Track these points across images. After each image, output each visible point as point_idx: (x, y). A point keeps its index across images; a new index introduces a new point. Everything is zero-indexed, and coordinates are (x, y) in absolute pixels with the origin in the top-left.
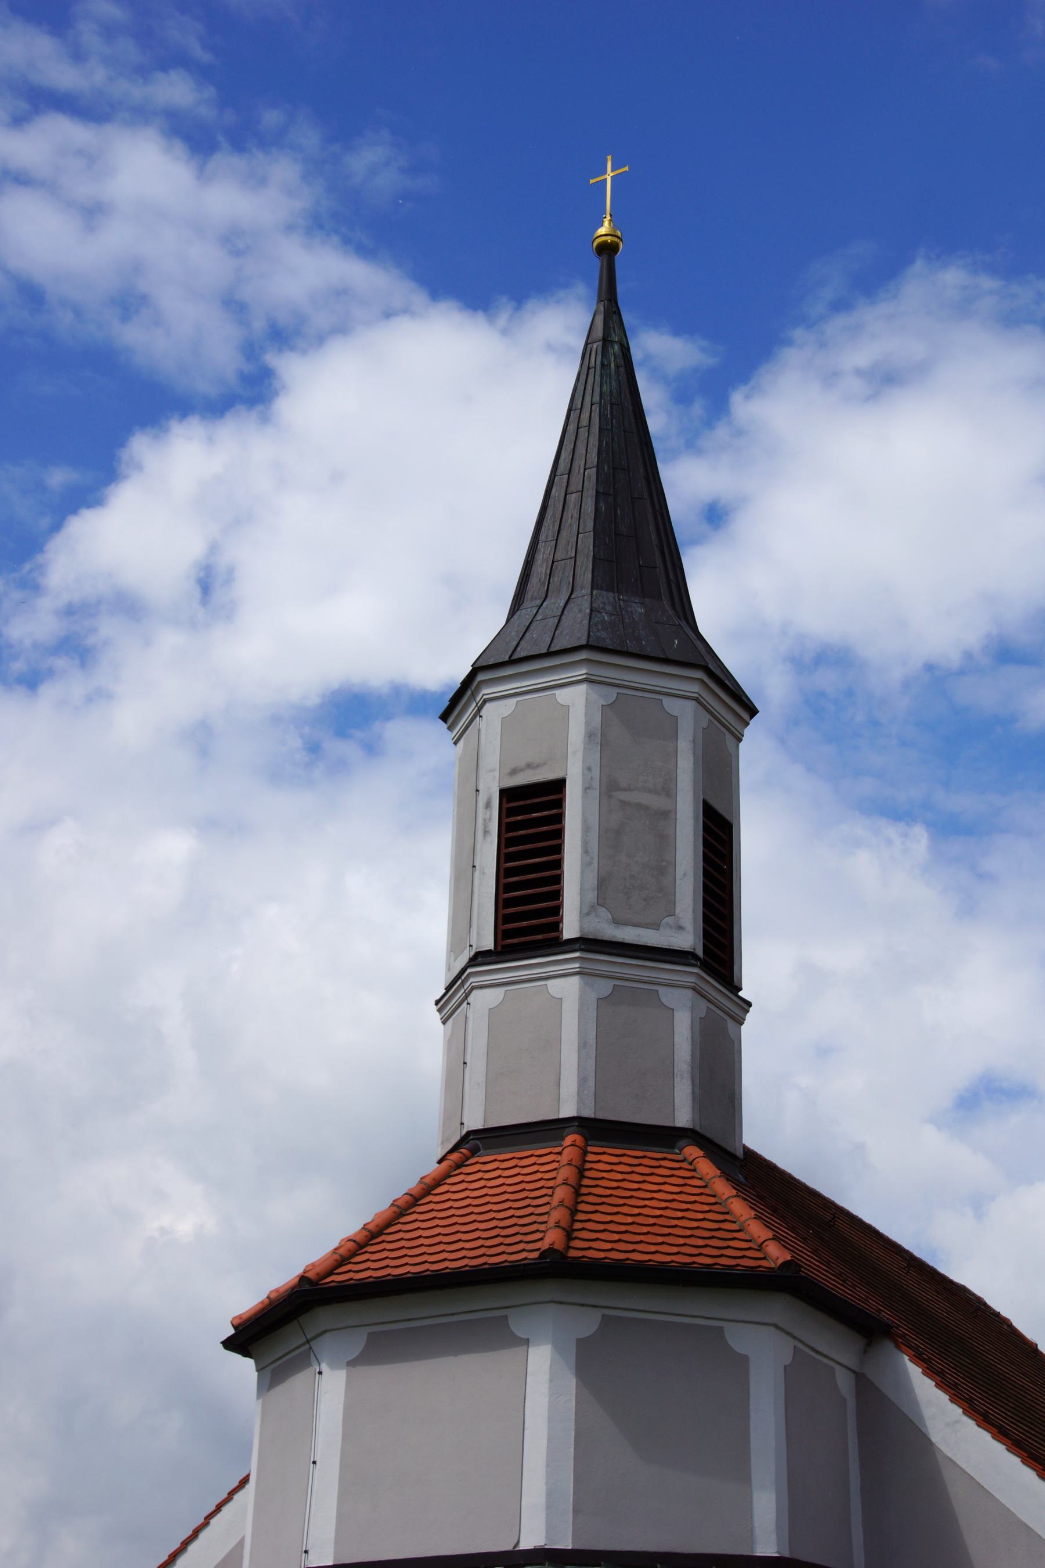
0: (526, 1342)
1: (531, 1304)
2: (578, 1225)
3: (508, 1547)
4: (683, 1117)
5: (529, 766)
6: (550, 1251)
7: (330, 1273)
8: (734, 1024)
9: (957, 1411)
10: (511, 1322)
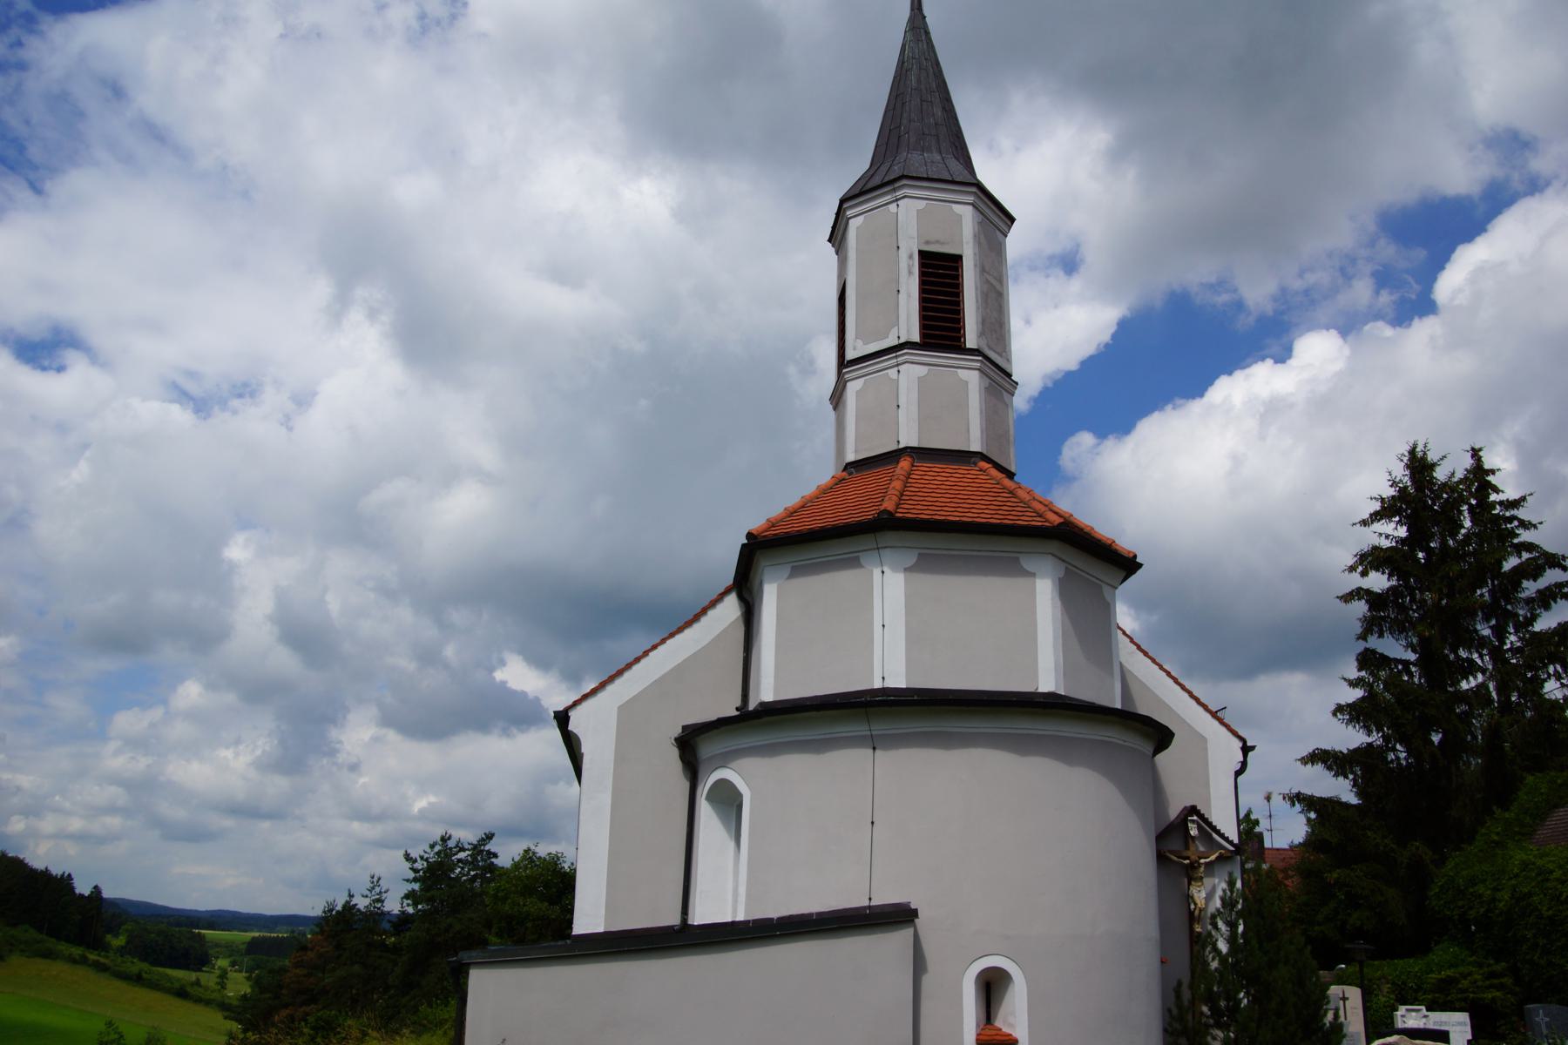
0: (1033, 575)
1: (865, 550)
2: (902, 502)
3: (1033, 690)
4: (975, 446)
5: (937, 242)
6: (885, 511)
7: (763, 532)
8: (1009, 395)
9: (686, 657)
10: (862, 561)
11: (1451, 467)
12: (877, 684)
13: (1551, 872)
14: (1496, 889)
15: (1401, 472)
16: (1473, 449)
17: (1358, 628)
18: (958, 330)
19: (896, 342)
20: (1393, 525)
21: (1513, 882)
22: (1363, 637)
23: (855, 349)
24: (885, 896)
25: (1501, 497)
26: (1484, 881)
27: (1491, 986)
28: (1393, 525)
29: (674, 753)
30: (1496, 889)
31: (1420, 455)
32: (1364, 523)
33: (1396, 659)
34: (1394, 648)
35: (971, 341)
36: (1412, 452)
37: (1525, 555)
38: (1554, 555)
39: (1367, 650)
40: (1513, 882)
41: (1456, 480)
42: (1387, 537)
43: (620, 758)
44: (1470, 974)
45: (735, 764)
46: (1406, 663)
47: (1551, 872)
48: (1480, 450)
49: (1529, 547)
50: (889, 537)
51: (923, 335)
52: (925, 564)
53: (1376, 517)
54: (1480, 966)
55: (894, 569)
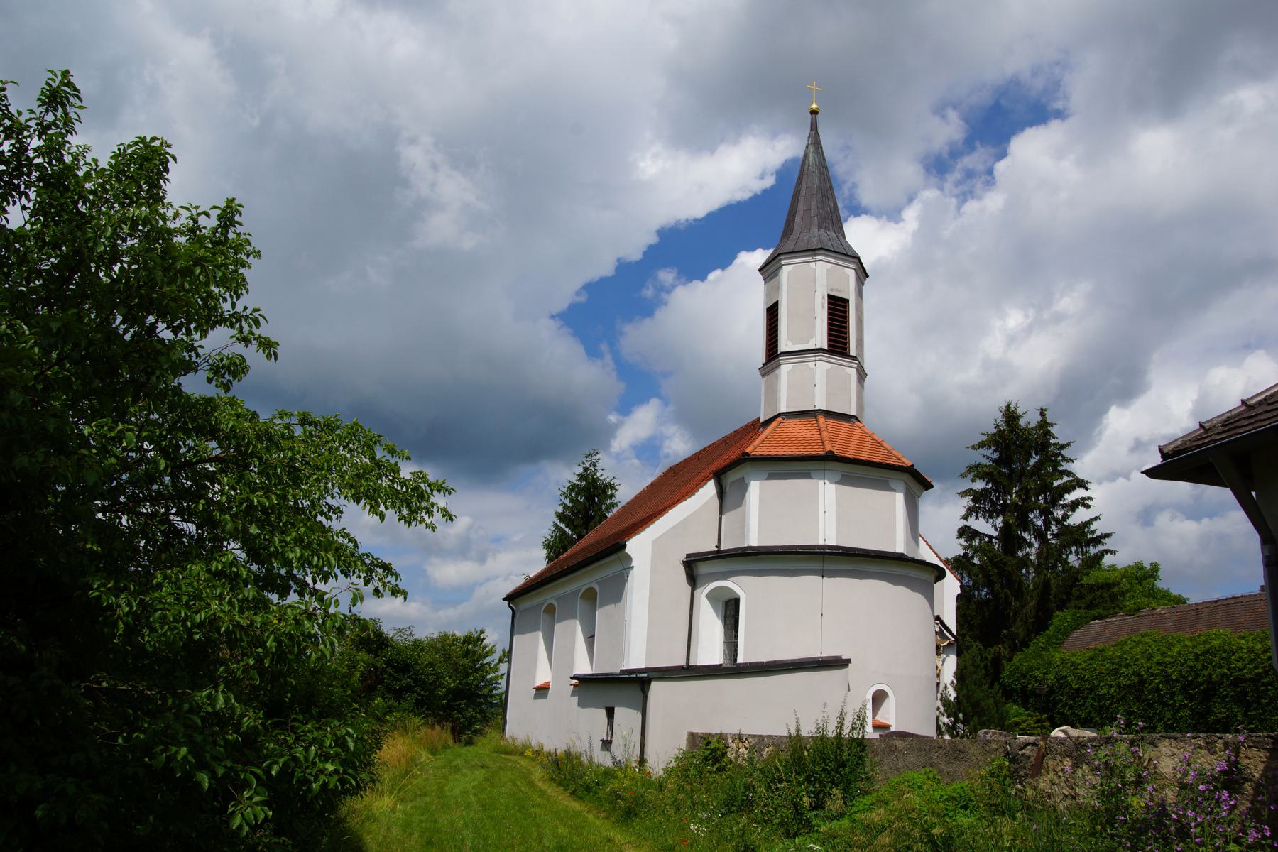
5: (837, 290)
11: (1030, 419)
12: (821, 542)
13: (1080, 664)
14: (1046, 673)
15: (1000, 419)
16: (1042, 409)
17: (963, 512)
18: (845, 344)
19: (814, 347)
20: (991, 451)
21: (1057, 670)
22: (965, 518)
23: (786, 346)
24: (829, 652)
25: (1056, 441)
26: (1038, 669)
27: (1038, 727)
28: (991, 451)
29: (682, 571)
30: (1046, 673)
31: (1012, 409)
32: (974, 448)
33: (984, 534)
34: (983, 526)
35: (852, 353)
36: (1008, 406)
37: (1066, 479)
38: (1082, 480)
39: (966, 526)
40: (1057, 670)
41: (1031, 427)
42: (988, 458)
43: (654, 570)
44: (1026, 721)
45: (733, 579)
46: (990, 537)
47: (1080, 664)
48: (1045, 410)
49: (1069, 473)
50: (830, 465)
51: (829, 345)
52: (845, 480)
53: (982, 445)
54: (1032, 716)
55: (831, 482)
